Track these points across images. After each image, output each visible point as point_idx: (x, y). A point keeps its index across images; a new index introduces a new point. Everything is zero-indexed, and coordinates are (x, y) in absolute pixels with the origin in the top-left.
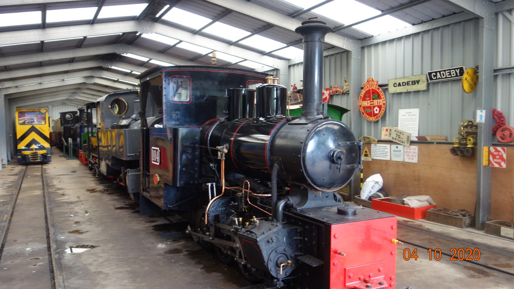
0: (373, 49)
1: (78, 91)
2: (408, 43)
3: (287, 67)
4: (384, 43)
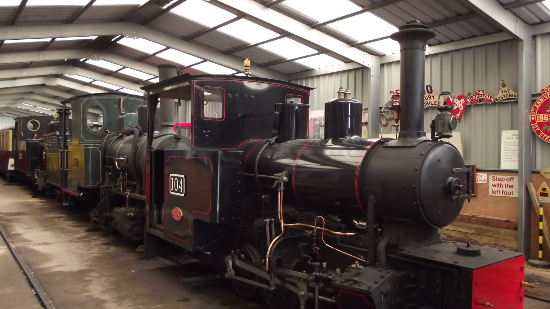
0: (315, 79)
1: (27, 97)
2: (345, 77)
3: (379, 66)
4: (324, 75)
